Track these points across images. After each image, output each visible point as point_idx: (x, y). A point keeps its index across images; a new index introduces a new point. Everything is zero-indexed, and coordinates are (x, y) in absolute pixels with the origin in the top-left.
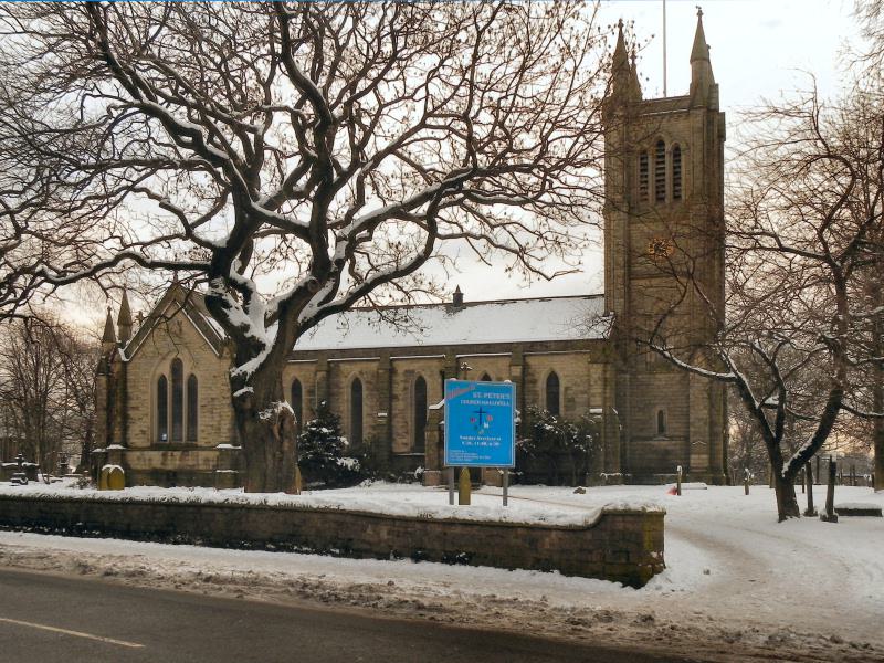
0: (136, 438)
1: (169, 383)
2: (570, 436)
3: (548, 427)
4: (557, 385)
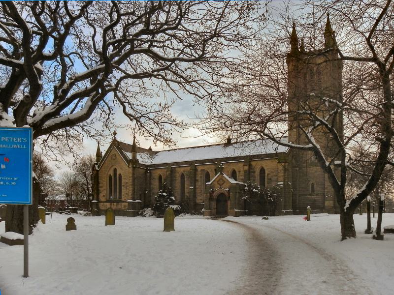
0: (102, 199)
1: (112, 177)
2: (267, 194)
3: (255, 190)
4: (264, 173)
